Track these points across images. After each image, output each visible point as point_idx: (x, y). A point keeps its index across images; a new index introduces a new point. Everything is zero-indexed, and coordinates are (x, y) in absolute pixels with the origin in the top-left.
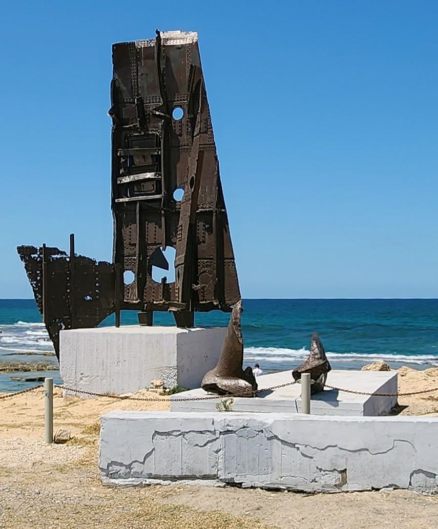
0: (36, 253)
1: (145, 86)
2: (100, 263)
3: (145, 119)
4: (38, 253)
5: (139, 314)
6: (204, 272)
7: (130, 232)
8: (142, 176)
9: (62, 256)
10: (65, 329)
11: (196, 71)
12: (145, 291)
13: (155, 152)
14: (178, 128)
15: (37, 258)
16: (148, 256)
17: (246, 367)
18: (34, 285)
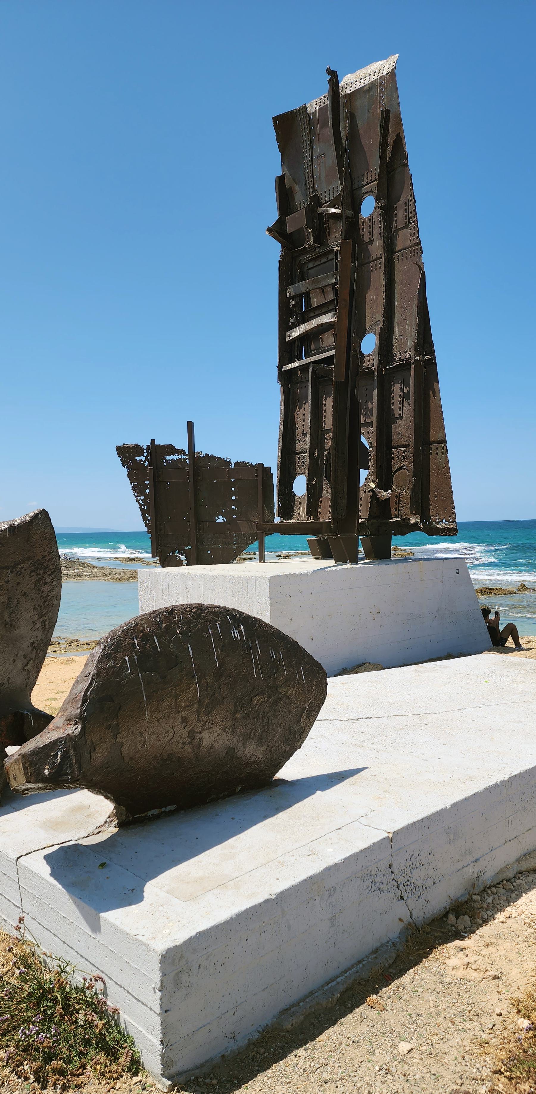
0: (142, 454)
1: (323, 175)
2: (237, 464)
3: (321, 225)
4: (145, 454)
5: (308, 540)
6: (400, 469)
7: (304, 414)
8: (314, 323)
9: (180, 457)
10: (187, 565)
11: (390, 121)
12: (320, 504)
13: (332, 279)
14: (367, 230)
15: (144, 462)
16: (325, 450)
17: (504, 626)
18: (141, 502)
